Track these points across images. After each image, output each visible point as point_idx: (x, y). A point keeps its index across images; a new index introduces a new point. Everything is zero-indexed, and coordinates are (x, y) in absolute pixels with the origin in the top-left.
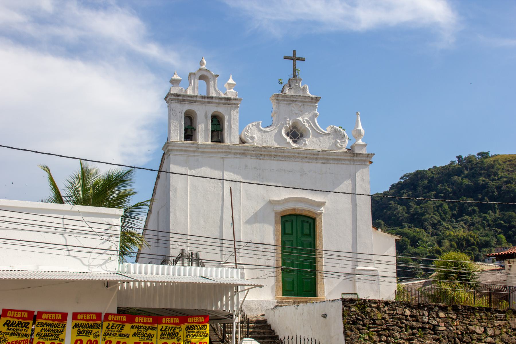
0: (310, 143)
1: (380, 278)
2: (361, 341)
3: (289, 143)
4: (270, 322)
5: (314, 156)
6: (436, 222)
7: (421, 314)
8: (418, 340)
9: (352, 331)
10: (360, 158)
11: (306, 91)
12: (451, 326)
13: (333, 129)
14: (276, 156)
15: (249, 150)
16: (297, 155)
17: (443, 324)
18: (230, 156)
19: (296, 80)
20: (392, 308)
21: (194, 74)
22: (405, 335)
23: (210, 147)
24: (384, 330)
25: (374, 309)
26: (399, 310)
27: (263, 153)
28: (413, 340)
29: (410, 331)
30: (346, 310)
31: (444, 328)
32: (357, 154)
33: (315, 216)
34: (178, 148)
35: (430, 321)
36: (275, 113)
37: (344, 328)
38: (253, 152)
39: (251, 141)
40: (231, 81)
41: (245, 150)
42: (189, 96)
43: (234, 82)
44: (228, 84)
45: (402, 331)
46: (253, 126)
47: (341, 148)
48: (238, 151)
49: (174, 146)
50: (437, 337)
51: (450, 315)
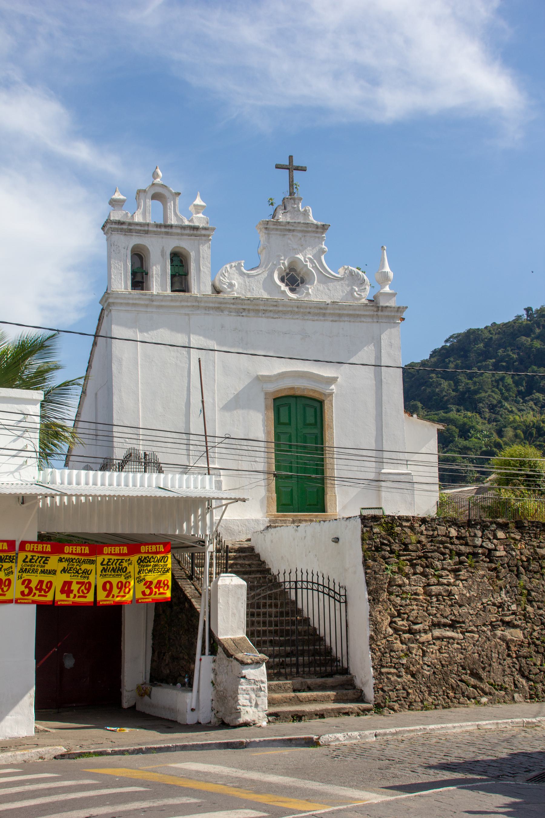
0: (315, 293)
2: (388, 574)
3: (284, 292)
5: (321, 311)
6: (495, 402)
7: (472, 534)
8: (468, 571)
9: (375, 560)
11: (309, 215)
13: (347, 272)
15: (226, 303)
16: (296, 309)
17: (502, 547)
18: (199, 312)
20: (432, 527)
21: (145, 191)
22: (449, 564)
23: (170, 298)
24: (420, 557)
25: (406, 529)
26: (442, 530)
27: (246, 307)
28: (461, 571)
30: (367, 531)
31: (503, 553)
32: (382, 307)
34: (122, 301)
35: (484, 544)
36: (264, 248)
37: (364, 556)
38: (232, 306)
40: (198, 201)
41: (221, 303)
43: (203, 204)
45: (444, 559)
46: (231, 267)
47: (360, 299)
48: (211, 305)
49: (116, 298)
50: (493, 566)
51: (512, 535)
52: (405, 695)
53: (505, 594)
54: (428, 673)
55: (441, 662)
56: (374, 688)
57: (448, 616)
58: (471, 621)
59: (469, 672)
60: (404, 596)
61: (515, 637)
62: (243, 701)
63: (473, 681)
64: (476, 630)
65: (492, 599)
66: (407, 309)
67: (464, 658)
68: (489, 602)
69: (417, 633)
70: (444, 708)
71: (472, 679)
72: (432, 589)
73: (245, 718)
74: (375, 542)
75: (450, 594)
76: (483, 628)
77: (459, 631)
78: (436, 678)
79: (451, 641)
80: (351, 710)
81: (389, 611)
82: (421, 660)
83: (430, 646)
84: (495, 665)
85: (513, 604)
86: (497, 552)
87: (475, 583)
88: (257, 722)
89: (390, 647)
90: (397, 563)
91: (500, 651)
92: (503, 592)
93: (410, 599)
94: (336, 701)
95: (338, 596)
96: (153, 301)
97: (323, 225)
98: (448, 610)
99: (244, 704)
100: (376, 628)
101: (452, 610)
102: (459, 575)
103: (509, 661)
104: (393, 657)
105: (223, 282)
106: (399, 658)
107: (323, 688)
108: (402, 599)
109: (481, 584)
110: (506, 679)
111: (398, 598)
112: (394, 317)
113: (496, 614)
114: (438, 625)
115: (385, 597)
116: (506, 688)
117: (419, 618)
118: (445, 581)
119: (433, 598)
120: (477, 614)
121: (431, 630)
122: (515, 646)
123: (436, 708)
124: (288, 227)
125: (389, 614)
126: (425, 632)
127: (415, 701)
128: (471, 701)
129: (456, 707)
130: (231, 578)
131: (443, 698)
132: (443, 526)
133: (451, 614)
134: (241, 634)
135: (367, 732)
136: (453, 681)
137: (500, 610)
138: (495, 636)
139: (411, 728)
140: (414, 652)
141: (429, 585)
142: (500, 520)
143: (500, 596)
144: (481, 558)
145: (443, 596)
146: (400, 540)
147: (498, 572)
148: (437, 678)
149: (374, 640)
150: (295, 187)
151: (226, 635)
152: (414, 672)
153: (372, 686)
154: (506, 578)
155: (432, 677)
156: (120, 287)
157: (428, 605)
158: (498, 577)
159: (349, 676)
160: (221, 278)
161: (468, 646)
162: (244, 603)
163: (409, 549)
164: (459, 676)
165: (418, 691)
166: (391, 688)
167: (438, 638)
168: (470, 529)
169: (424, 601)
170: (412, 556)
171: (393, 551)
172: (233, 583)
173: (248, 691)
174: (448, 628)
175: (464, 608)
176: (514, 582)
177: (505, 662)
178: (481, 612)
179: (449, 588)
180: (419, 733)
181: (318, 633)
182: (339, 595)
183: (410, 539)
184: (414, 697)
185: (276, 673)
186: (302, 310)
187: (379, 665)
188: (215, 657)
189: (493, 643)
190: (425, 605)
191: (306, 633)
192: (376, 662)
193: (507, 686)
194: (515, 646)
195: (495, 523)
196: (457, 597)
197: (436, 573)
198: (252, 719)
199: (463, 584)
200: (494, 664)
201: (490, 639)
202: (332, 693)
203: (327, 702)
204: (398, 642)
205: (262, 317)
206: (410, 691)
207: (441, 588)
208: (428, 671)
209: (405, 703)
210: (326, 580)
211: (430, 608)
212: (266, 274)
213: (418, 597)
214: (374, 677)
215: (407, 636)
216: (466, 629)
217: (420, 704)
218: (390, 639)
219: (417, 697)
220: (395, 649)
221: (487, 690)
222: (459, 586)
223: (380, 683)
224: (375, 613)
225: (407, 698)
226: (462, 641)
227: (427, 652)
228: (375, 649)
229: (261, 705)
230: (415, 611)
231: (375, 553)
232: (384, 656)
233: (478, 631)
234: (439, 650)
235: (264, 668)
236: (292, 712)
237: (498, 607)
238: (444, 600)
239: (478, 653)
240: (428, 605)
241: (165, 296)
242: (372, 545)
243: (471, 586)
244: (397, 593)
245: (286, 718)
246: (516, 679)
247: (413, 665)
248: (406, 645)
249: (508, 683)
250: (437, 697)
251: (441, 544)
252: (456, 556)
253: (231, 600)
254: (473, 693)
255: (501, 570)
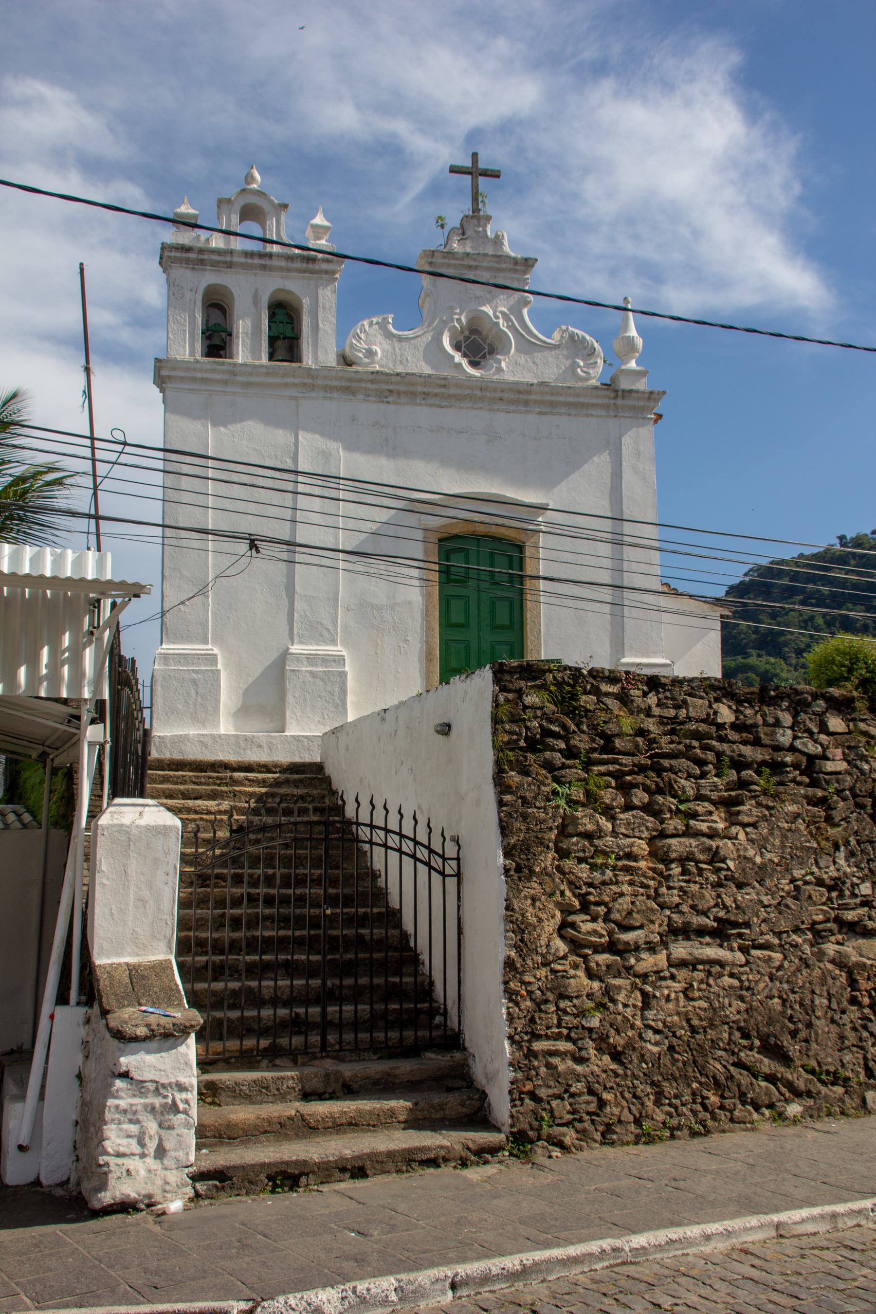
0: (510, 368)
1: (627, 594)
2: (557, 807)
3: (459, 365)
4: (329, 770)
5: (521, 397)
6: (803, 646)
7: (771, 720)
8: (759, 804)
9: (525, 772)
10: (631, 403)
11: (502, 244)
12: (864, 758)
13: (566, 335)
14: (426, 395)
15: (360, 381)
16: (479, 393)
17: (839, 751)
18: (313, 395)
19: (478, 218)
20: (673, 699)
21: (229, 201)
22: (715, 788)
23: (264, 370)
24: (642, 769)
25: (609, 701)
26: (698, 706)
27: (393, 388)
28: (742, 803)
29: (732, 775)
30: (507, 700)
31: (842, 766)
32: (623, 391)
33: (522, 537)
34: (183, 374)
35: (798, 743)
36: (427, 296)
37: (498, 763)
38: (369, 385)
39: (366, 360)
40: (319, 220)
41: (350, 380)
42: (214, 251)
43: (326, 223)
44: (313, 226)
45: (703, 775)
46: (371, 324)
47: (587, 380)
48: (335, 383)
49: (174, 369)
50: (820, 793)
51: (862, 725)
52: (593, 1107)
53: (847, 859)
54: (655, 1049)
55: (688, 1021)
56: (510, 1092)
57: (709, 909)
58: (764, 921)
59: (757, 1043)
60: (599, 861)
61: (869, 959)
62: (119, 1141)
63: (767, 1065)
64: (776, 941)
65: (815, 869)
66: (665, 397)
67: (747, 1010)
68: (808, 878)
69: (630, 951)
70: (694, 1134)
71: (766, 1060)
72: (670, 846)
73: (119, 1188)
74: (527, 728)
75: (715, 857)
76: (794, 937)
77: (735, 945)
78: (674, 1061)
79: (716, 969)
80: (442, 1153)
81: (558, 897)
82: (638, 1017)
83: (663, 983)
84: (821, 1024)
85: (863, 881)
86: (829, 763)
87: (776, 832)
88: (158, 1198)
89: (559, 986)
90: (585, 780)
91: (833, 991)
92: (841, 855)
93: (614, 868)
94: (414, 1123)
95: (440, 860)
96: (235, 375)
97: (526, 260)
98: (709, 895)
99: (122, 1149)
100: (522, 940)
101: (719, 896)
102: (738, 813)
103: (854, 1013)
104: (565, 1012)
105: (358, 346)
106: (582, 1013)
107: (384, 1087)
108: (593, 867)
109: (789, 834)
110: (848, 1058)
111: (583, 865)
112: (643, 409)
113: (824, 904)
114: (685, 932)
115: (549, 863)
116: (847, 1080)
117: (635, 915)
118: (704, 827)
119: (673, 866)
120: (779, 904)
121: (665, 944)
122: (869, 979)
123: (672, 1137)
124: (466, 262)
125: (558, 904)
126: (652, 948)
127: (620, 1121)
128: (763, 1114)
129: (724, 1131)
130: (140, 809)
131: (691, 1110)
132: (701, 698)
133: (716, 905)
134: (163, 953)
135: (424, 1277)
136: (719, 1067)
137: (834, 894)
138: (820, 955)
139: (573, 1250)
140: (621, 997)
141: (663, 835)
142: (835, 691)
143: (834, 863)
144: (791, 775)
145: (697, 862)
146: (593, 727)
147: (830, 808)
148: (678, 1060)
149: (516, 969)
150: (480, 199)
151: (118, 954)
152: (619, 1049)
153: (507, 1086)
154: (848, 822)
155: (666, 1060)
156: (182, 352)
157: (660, 884)
158: (829, 819)
159: (458, 1055)
160: (354, 341)
161: (756, 982)
162: (171, 871)
163: (614, 748)
164: (733, 1053)
165: (628, 1095)
166: (556, 1091)
167: (683, 964)
168: (765, 708)
169: (650, 874)
170: (621, 765)
171: (575, 750)
172: (142, 822)
173: (135, 1113)
174: (707, 939)
175: (748, 890)
176: (867, 832)
177: (844, 1016)
178: (789, 901)
179: (714, 844)
180: (598, 1266)
181: (412, 944)
182: (442, 857)
183: (618, 724)
184: (616, 1111)
185: (265, 1049)
186: (488, 394)
187: (526, 1033)
188: (89, 1011)
189: (817, 972)
190: (651, 883)
191: (382, 944)
192: (520, 1025)
193: (849, 1074)
194: (869, 979)
195: (823, 696)
196: (731, 864)
197: (682, 807)
198: (143, 1192)
199: (747, 834)
200: (818, 1022)
201: (810, 962)
202: (400, 1105)
203: (387, 1128)
204: (581, 973)
205: (420, 404)
206: (606, 1096)
207: (694, 842)
208: (656, 1044)
209: (592, 1128)
210: (379, 813)
211: (664, 890)
212: (429, 337)
213: (633, 864)
214: (511, 1064)
215: (603, 958)
216: (753, 940)
217: (632, 1127)
218: (559, 967)
219: (626, 1110)
220: (572, 991)
221: (801, 1085)
222: (736, 838)
223: (529, 1079)
224: (522, 904)
225: (598, 1115)
226: (742, 969)
227: (655, 996)
228: (517, 993)
229: (175, 1150)
230: (626, 897)
231: (528, 755)
232: (541, 1011)
233: (781, 945)
234: (685, 992)
235: (190, 1048)
236: (270, 1165)
237: (830, 889)
238: (700, 871)
239: (780, 997)
240: (660, 883)
241: (255, 366)
242: (519, 734)
243: (766, 839)
244: (581, 854)
245: (251, 1182)
246: (869, 1056)
247: (618, 1031)
248: (601, 981)
249: (851, 1066)
250: (676, 1108)
251: (697, 739)
252: (730, 768)
253: (133, 866)
254: (768, 1093)
255: (837, 802)
